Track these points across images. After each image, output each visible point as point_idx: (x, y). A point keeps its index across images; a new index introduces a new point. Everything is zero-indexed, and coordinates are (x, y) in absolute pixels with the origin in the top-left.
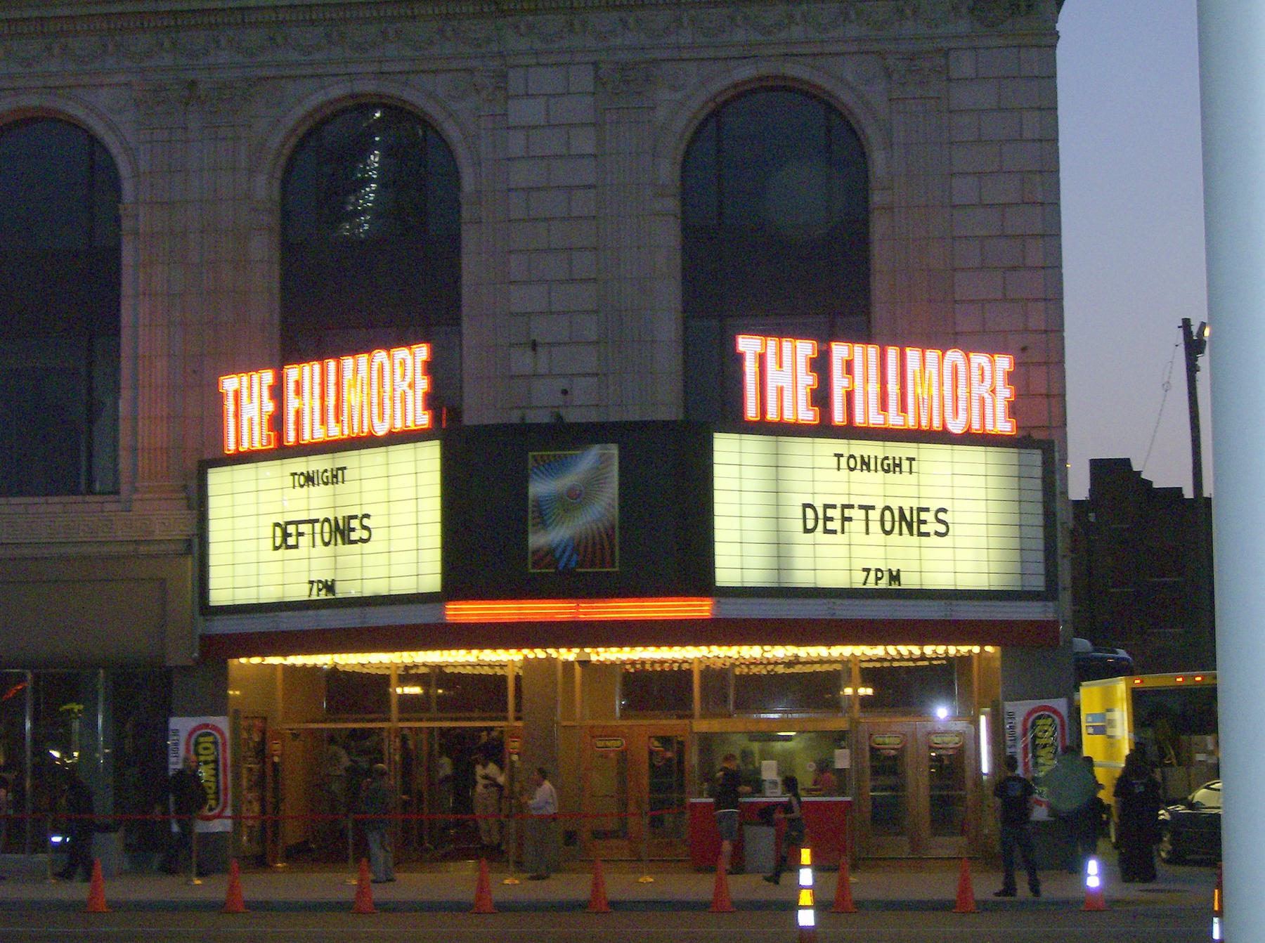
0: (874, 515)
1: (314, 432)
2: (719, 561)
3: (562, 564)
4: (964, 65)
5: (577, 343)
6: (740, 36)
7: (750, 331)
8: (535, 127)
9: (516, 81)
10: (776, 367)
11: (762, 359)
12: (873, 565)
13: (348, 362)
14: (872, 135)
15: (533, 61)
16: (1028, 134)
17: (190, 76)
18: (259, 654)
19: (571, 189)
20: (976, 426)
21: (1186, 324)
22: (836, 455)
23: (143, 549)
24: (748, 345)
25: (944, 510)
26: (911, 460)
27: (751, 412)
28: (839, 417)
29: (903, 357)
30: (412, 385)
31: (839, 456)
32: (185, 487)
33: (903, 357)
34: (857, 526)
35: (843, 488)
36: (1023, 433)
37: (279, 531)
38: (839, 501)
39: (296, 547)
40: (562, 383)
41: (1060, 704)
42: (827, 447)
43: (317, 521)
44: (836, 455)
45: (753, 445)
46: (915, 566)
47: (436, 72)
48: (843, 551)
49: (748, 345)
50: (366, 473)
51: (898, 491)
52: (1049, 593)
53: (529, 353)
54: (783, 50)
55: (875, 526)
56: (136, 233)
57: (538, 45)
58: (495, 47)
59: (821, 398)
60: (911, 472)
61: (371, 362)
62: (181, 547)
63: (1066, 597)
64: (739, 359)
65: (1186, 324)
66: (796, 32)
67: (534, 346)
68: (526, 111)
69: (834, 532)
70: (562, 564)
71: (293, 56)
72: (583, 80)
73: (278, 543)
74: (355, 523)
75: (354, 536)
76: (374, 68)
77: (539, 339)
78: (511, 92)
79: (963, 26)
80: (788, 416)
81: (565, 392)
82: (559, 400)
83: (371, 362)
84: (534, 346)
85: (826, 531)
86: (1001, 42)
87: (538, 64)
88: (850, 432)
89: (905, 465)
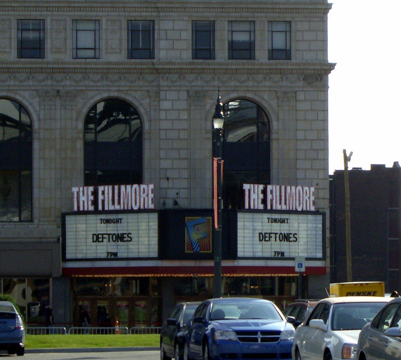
0: (278, 236)
1: (109, 206)
2: (239, 250)
3: (195, 250)
4: (301, 96)
5: (181, 178)
6: (233, 83)
7: (247, 183)
8: (169, 110)
9: (162, 94)
10: (253, 193)
11: (249, 190)
12: (277, 250)
13: (123, 187)
14: (273, 117)
15: (168, 89)
16: (319, 118)
17: (58, 88)
18: (100, 274)
19: (180, 130)
20: (305, 209)
21: (345, 151)
22: (268, 218)
23: (43, 240)
24: (246, 187)
25: (296, 234)
26: (287, 219)
27: (247, 207)
28: (269, 207)
29: (286, 188)
30: (147, 196)
31: (269, 218)
32: (56, 221)
33: (286, 188)
34: (273, 239)
35: (269, 228)
36: (317, 210)
37: (95, 237)
38: (269, 232)
39: (102, 241)
40: (177, 191)
41: (116, 286)
42: (266, 216)
43: (111, 234)
44: (268, 218)
45: (248, 216)
46: (288, 251)
47: (136, 91)
48: (269, 246)
49: (246, 187)
50: (130, 220)
51: (284, 228)
52: (324, 259)
53: (166, 181)
54: (246, 89)
55: (278, 239)
56: (39, 139)
57: (170, 84)
58: (155, 84)
59: (264, 201)
60: (287, 223)
61: (131, 187)
62: (56, 240)
63: (328, 260)
64: (244, 191)
65: (345, 151)
66: (250, 83)
67: (168, 179)
68: (166, 105)
69: (267, 241)
70: (195, 250)
71: (91, 84)
72: (184, 95)
73: (95, 240)
74: (125, 236)
75: (125, 239)
76: (117, 88)
77: (169, 177)
78: (161, 98)
79: (301, 83)
80: (256, 207)
81: (177, 194)
82: (175, 196)
83: (131, 187)
84: (168, 179)
85: (265, 241)
86: (312, 89)
87: (170, 90)
88: (272, 211)
89: (286, 221)
